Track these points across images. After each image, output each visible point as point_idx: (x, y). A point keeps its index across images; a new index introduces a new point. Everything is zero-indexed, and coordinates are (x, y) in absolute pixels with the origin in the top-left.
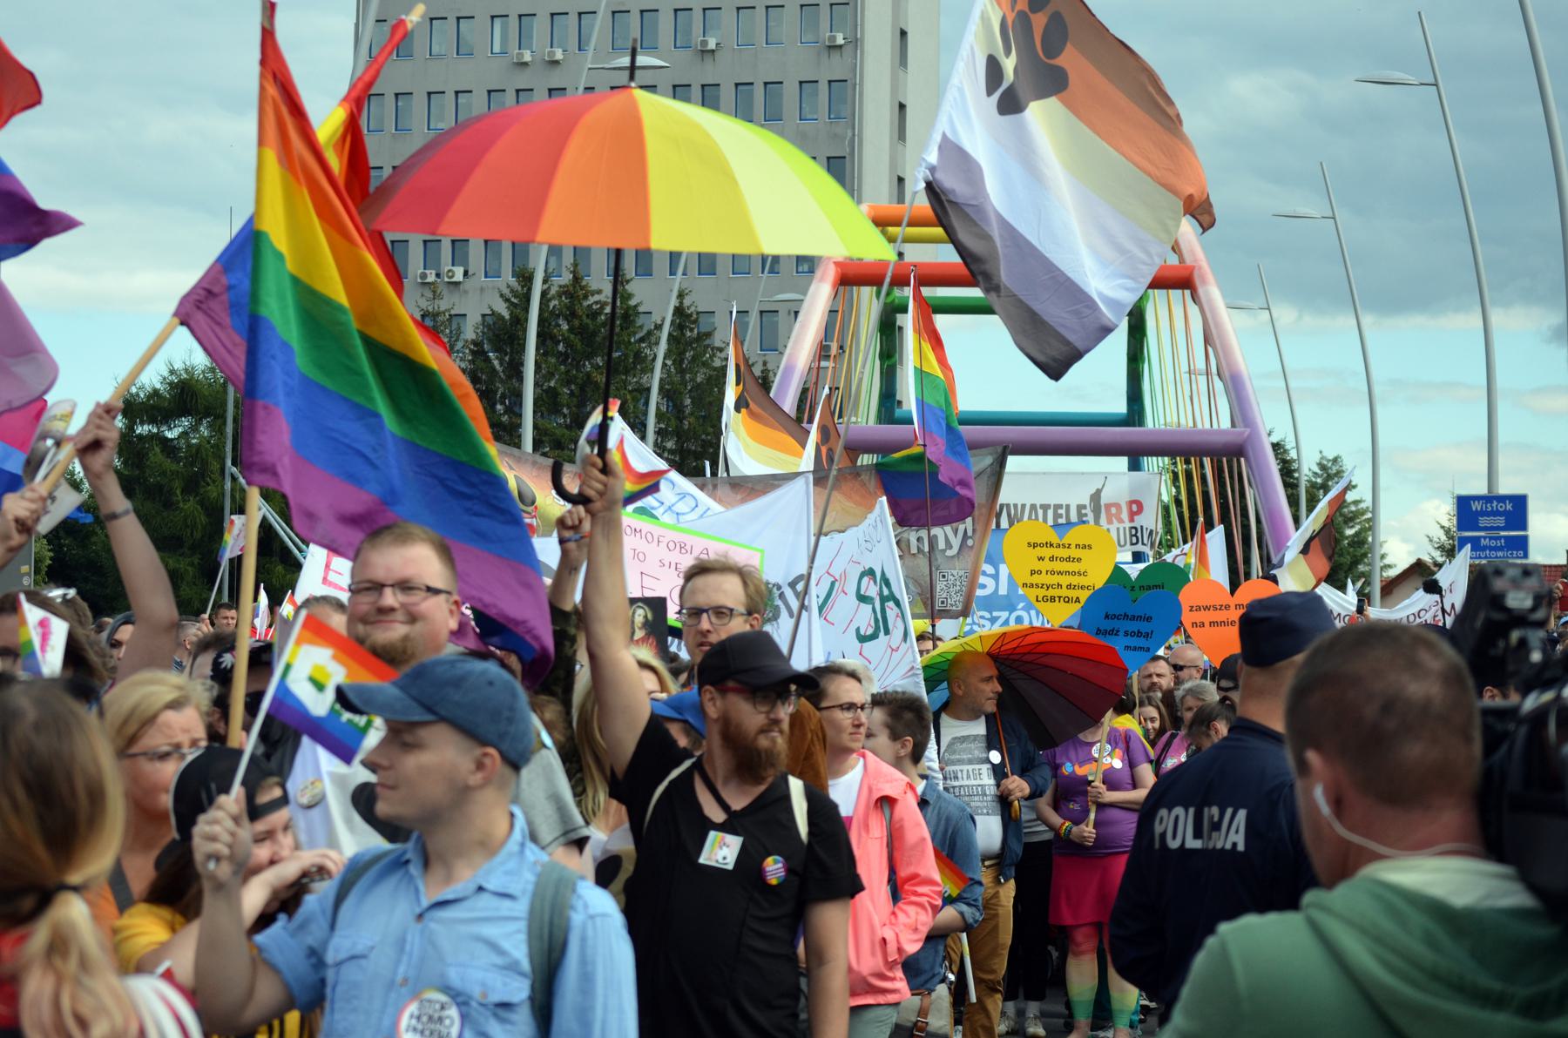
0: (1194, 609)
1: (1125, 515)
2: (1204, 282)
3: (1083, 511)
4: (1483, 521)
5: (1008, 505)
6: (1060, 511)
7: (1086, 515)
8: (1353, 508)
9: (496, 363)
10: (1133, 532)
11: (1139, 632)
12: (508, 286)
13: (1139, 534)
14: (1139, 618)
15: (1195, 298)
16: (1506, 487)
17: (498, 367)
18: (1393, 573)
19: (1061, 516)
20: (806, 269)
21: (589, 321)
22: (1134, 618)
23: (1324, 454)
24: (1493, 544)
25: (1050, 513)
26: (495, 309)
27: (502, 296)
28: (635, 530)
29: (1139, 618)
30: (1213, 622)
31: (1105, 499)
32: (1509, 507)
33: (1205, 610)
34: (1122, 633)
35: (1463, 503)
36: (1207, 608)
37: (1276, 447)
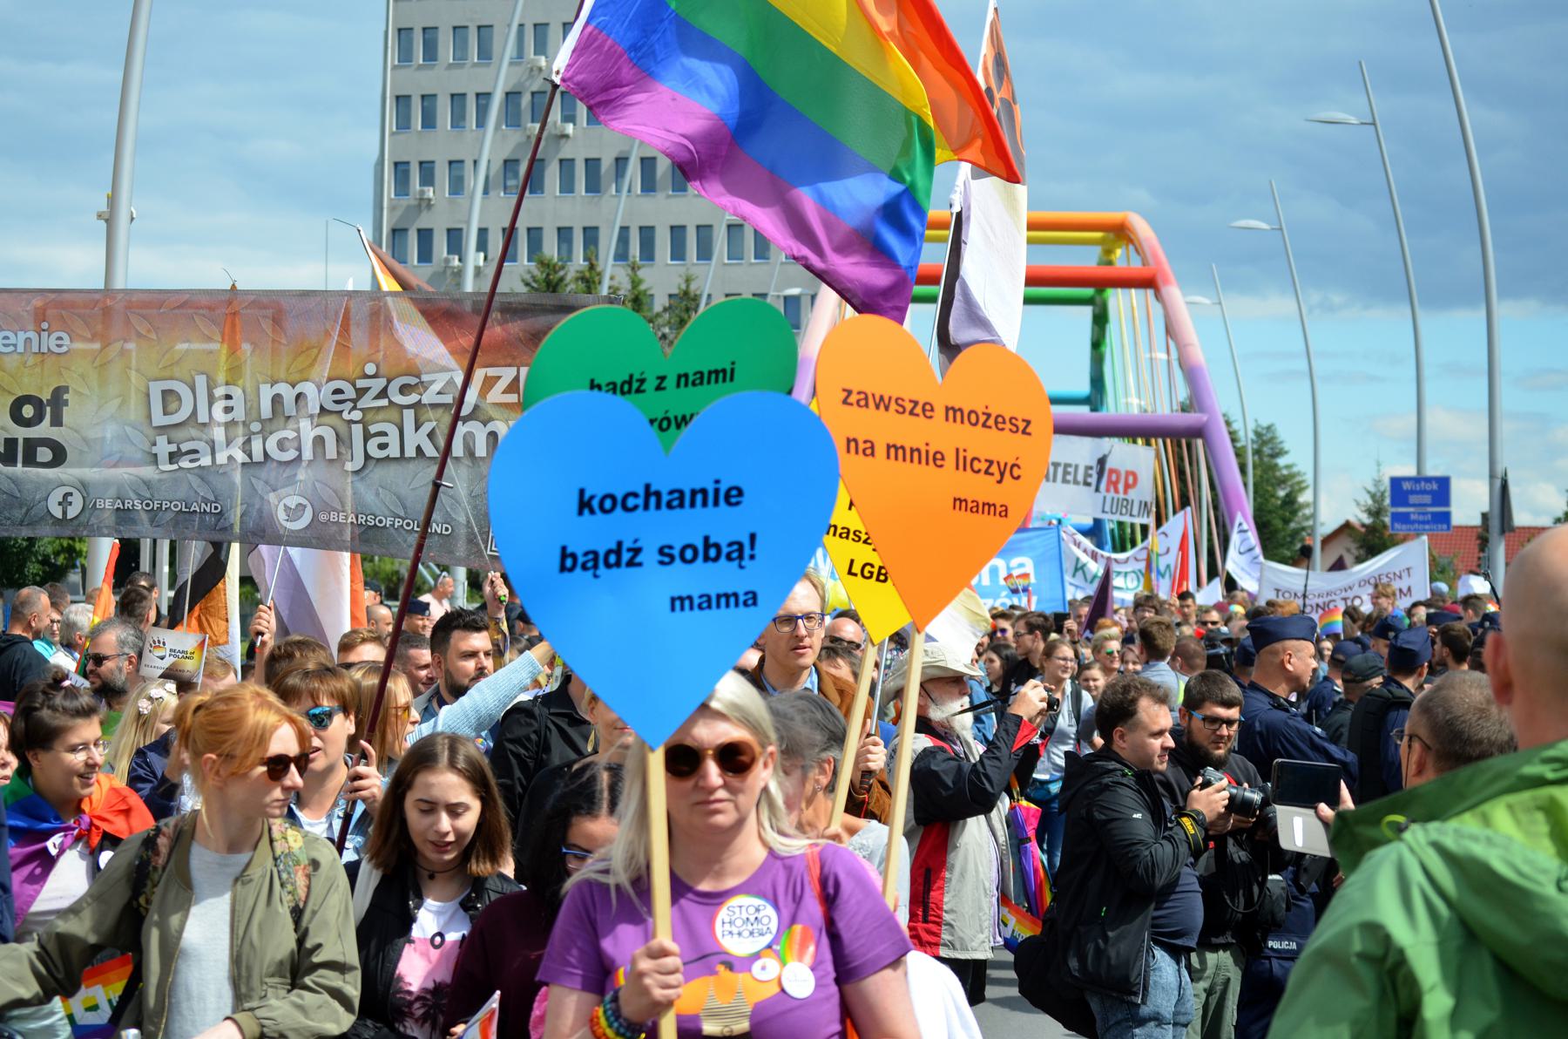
0: (853, 399)
1: (1121, 487)
2: (1166, 282)
3: (1090, 472)
4: (1413, 499)
6: (1069, 469)
7: (1091, 476)
8: (1285, 472)
11: (707, 544)
13: (1129, 507)
14: (700, 497)
16: (1431, 470)
19: (1069, 473)
22: (679, 499)
23: (1259, 422)
24: (1421, 518)
25: (1060, 470)
27: (523, 281)
28: (1295, 595)
29: (700, 497)
30: (682, 599)
32: (1435, 487)
33: (877, 407)
34: (649, 557)
36: (882, 403)
37: (1224, 415)
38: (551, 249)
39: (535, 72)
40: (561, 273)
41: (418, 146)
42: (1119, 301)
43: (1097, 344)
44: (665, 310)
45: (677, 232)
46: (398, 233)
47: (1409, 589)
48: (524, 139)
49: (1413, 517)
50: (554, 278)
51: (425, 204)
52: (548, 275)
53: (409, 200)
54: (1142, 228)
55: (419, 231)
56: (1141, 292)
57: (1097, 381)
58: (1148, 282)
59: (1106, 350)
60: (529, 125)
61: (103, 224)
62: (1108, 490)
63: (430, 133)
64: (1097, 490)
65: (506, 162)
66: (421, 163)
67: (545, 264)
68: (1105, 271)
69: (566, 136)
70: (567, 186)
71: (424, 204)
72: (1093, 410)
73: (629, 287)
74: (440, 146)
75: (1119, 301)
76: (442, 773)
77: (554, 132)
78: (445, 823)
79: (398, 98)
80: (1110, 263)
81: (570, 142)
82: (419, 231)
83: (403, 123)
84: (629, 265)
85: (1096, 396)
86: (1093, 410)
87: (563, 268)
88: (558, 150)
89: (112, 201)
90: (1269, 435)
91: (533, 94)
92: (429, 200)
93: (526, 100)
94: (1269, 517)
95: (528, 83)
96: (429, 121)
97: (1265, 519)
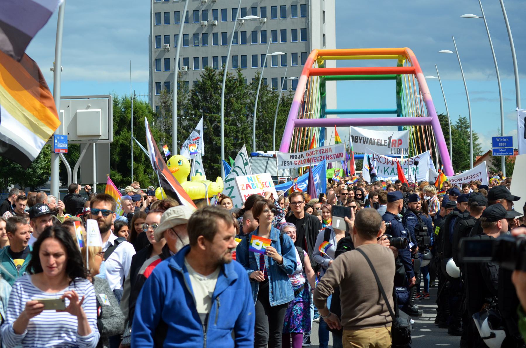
1: (397, 145)
4: (500, 144)
5: (363, 138)
9: (199, 97)
10: (398, 153)
12: (203, 73)
15: (416, 76)
17: (200, 98)
18: (483, 153)
20: (295, 64)
21: (229, 83)
24: (503, 151)
26: (199, 80)
27: (201, 76)
31: (393, 138)
32: (507, 140)
35: (494, 139)
38: (211, 64)
39: (204, 3)
40: (214, 72)
41: (164, 30)
42: (404, 77)
43: (398, 93)
44: (251, 84)
45: (254, 57)
46: (158, 60)
47: (481, 179)
48: (200, 26)
49: (500, 150)
50: (211, 74)
51: (167, 50)
52: (209, 73)
53: (161, 49)
54: (411, 53)
55: (165, 59)
56: (411, 75)
57: (399, 105)
58: (413, 72)
59: (401, 94)
60: (202, 21)
61: (52, 72)
62: (392, 146)
63: (167, 25)
64: (389, 147)
65: (194, 34)
66: (165, 36)
67: (208, 70)
68: (400, 68)
69: (215, 25)
70: (216, 42)
71: (166, 50)
72: (398, 116)
73: (238, 77)
74: (170, 30)
75: (404, 77)
76: (521, 238)
77: (210, 24)
78: (53, 260)
79: (156, 13)
80: (401, 65)
81: (216, 27)
82: (165, 59)
83: (158, 22)
84: (237, 69)
85: (399, 111)
86: (398, 116)
87: (214, 71)
88: (212, 30)
89: (55, 64)
90: (464, 121)
91: (203, 10)
92: (168, 48)
93: (200, 13)
94: (462, 150)
95: (201, 7)
96: (167, 21)
97: (460, 151)
